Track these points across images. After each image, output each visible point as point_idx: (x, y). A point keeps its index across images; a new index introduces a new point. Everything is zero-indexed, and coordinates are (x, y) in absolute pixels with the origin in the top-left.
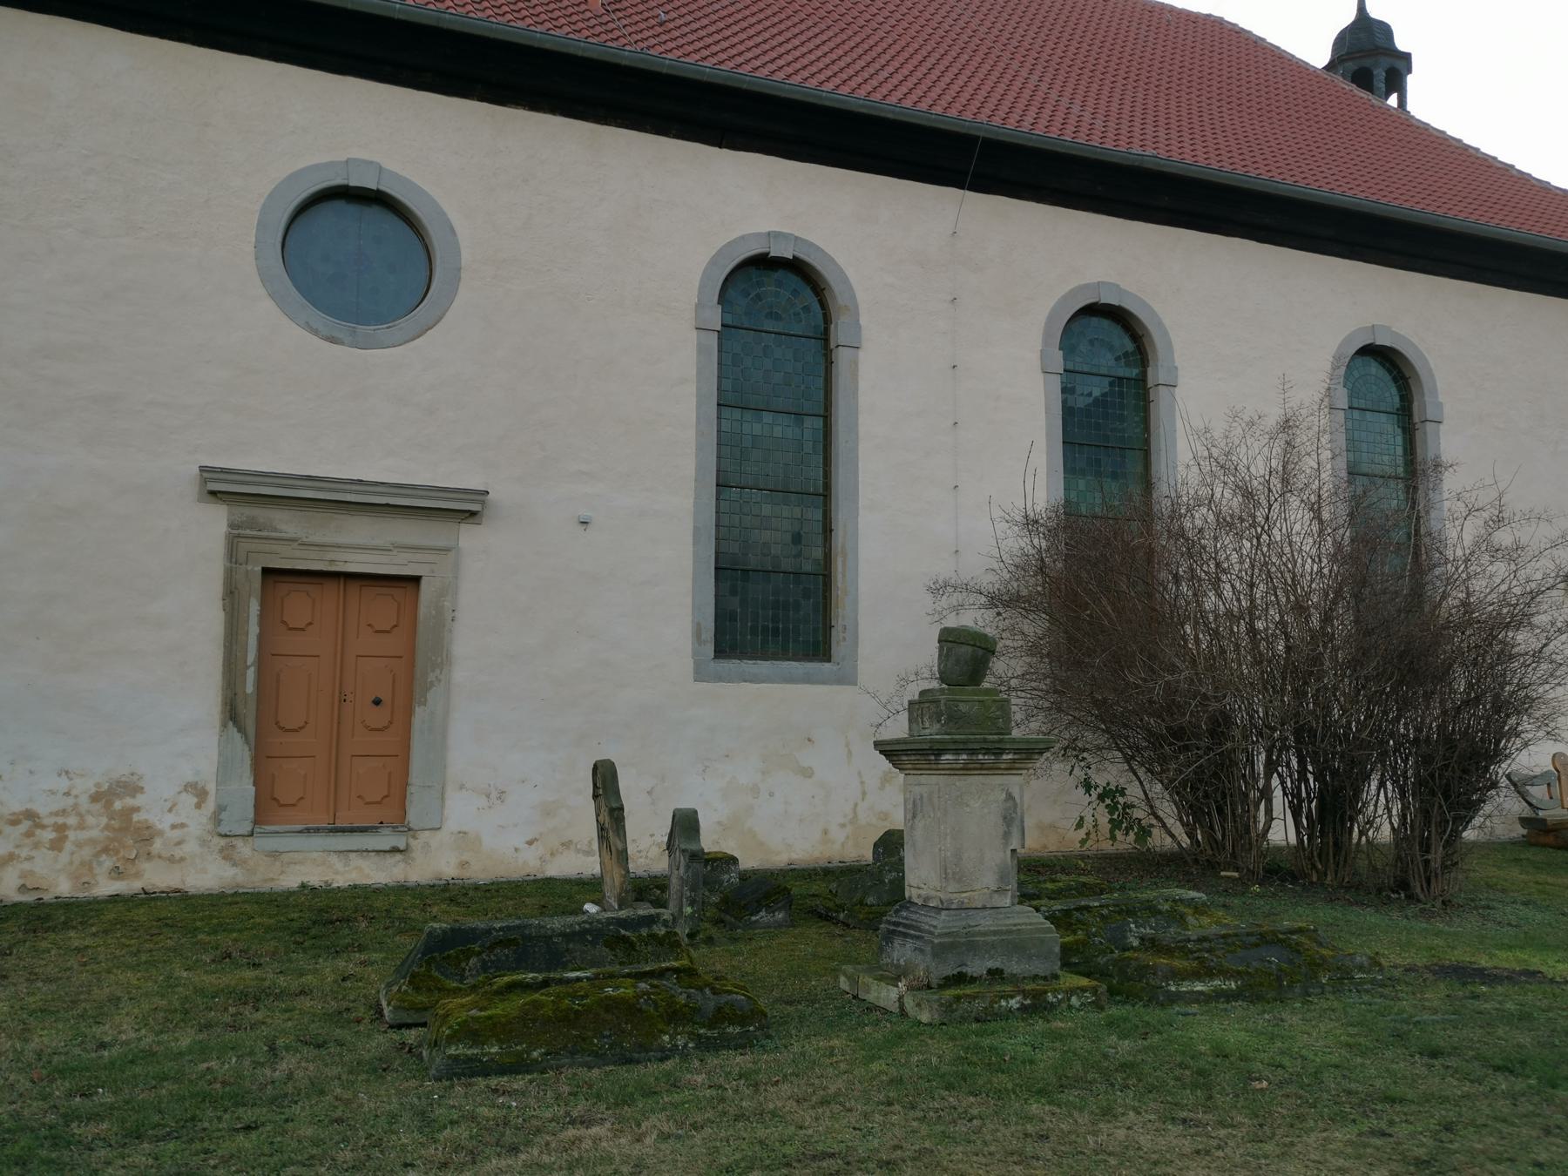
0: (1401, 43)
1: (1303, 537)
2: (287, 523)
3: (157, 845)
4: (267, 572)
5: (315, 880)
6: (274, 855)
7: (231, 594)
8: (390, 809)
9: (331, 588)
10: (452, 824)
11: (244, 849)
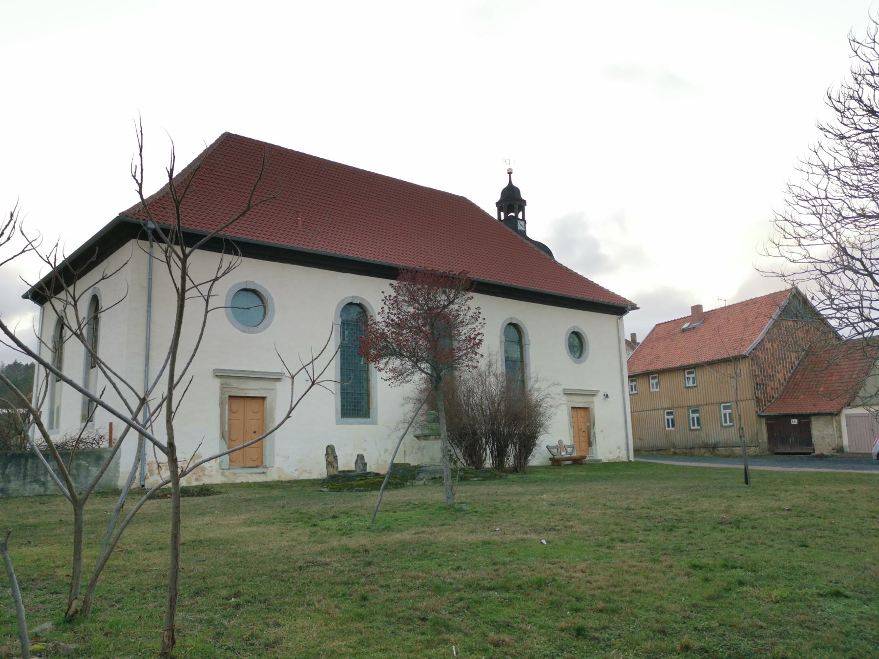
0: (523, 196)
1: (494, 385)
2: (234, 383)
3: (206, 472)
4: (230, 397)
5: (245, 481)
6: (235, 474)
7: (222, 404)
8: (259, 463)
9: (242, 400)
10: (276, 466)
11: (227, 473)
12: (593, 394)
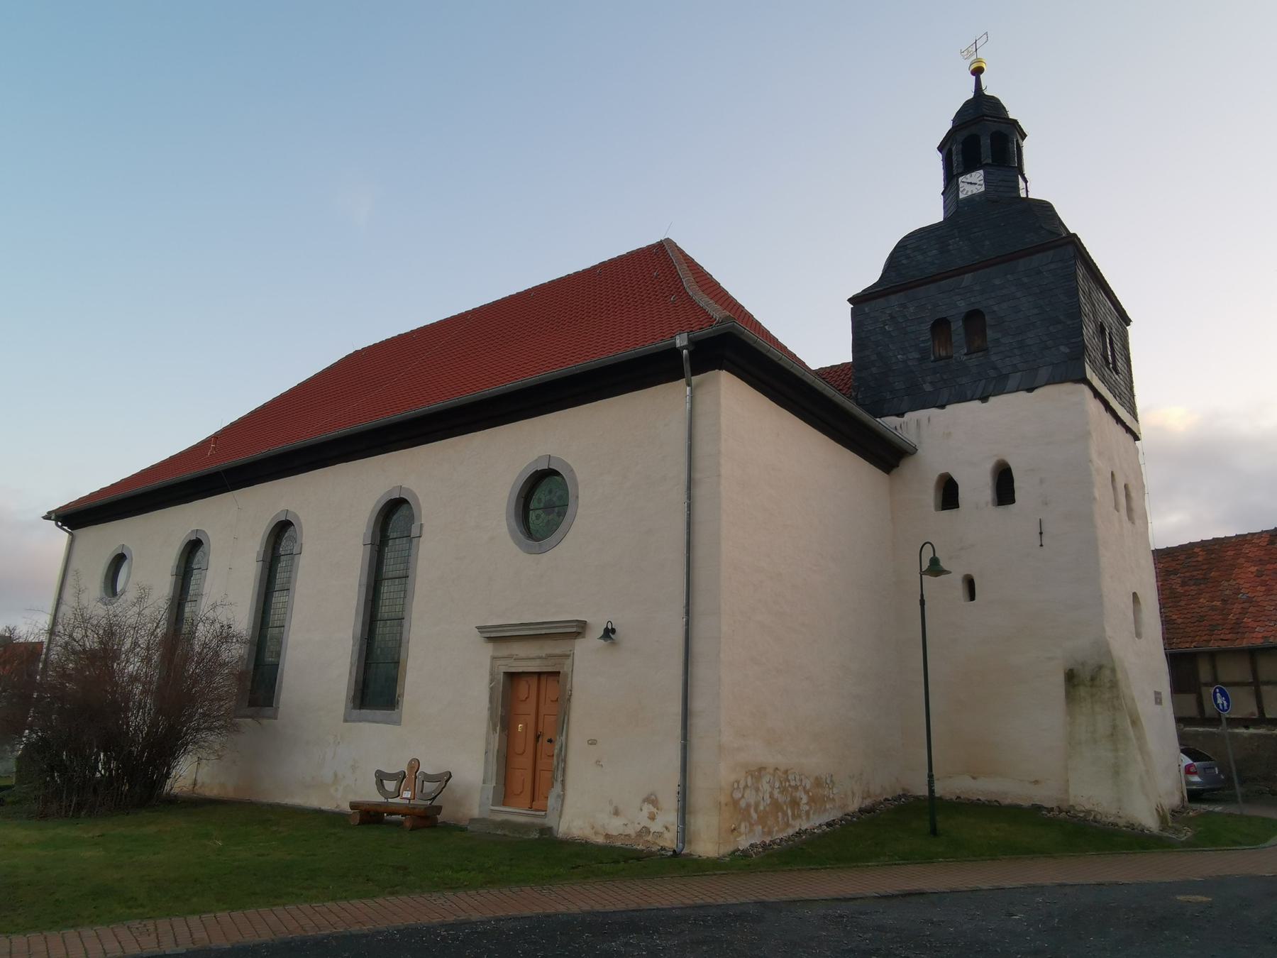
12: (578, 630)
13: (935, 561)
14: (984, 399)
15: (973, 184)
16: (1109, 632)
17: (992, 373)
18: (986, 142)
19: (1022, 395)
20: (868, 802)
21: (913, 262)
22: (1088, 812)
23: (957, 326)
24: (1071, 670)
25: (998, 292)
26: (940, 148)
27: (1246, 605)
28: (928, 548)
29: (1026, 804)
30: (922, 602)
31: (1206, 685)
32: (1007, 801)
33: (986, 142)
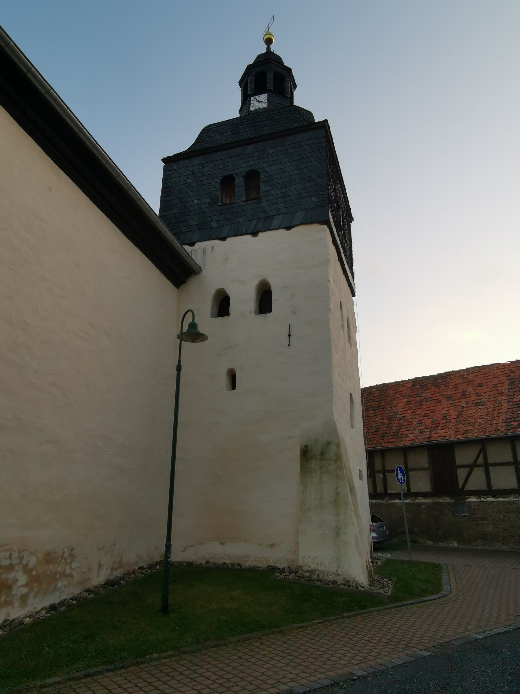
13: (193, 326)
14: (255, 234)
15: (260, 102)
16: (336, 416)
17: (262, 215)
18: (270, 78)
19: (283, 232)
20: (118, 573)
21: (213, 140)
22: (312, 572)
23: (240, 181)
24: (306, 447)
25: (272, 164)
26: (240, 83)
27: (402, 421)
28: (189, 316)
29: (263, 565)
30: (179, 368)
31: (379, 472)
32: (247, 564)
33: (270, 78)
